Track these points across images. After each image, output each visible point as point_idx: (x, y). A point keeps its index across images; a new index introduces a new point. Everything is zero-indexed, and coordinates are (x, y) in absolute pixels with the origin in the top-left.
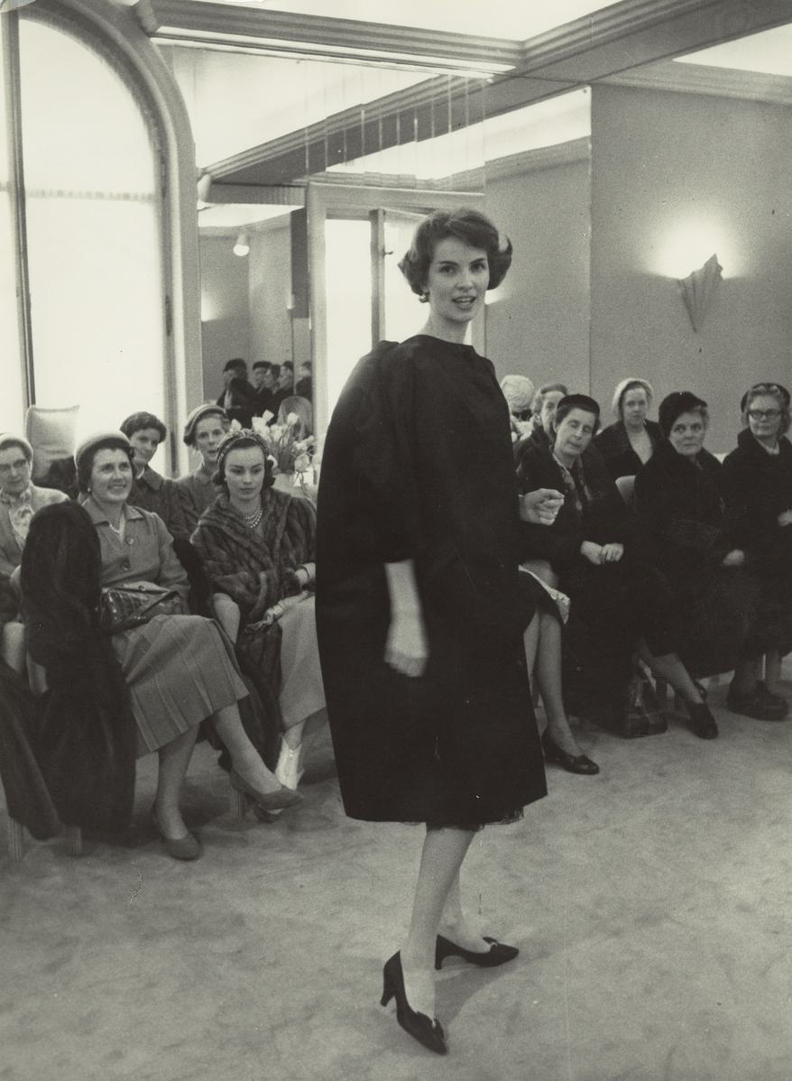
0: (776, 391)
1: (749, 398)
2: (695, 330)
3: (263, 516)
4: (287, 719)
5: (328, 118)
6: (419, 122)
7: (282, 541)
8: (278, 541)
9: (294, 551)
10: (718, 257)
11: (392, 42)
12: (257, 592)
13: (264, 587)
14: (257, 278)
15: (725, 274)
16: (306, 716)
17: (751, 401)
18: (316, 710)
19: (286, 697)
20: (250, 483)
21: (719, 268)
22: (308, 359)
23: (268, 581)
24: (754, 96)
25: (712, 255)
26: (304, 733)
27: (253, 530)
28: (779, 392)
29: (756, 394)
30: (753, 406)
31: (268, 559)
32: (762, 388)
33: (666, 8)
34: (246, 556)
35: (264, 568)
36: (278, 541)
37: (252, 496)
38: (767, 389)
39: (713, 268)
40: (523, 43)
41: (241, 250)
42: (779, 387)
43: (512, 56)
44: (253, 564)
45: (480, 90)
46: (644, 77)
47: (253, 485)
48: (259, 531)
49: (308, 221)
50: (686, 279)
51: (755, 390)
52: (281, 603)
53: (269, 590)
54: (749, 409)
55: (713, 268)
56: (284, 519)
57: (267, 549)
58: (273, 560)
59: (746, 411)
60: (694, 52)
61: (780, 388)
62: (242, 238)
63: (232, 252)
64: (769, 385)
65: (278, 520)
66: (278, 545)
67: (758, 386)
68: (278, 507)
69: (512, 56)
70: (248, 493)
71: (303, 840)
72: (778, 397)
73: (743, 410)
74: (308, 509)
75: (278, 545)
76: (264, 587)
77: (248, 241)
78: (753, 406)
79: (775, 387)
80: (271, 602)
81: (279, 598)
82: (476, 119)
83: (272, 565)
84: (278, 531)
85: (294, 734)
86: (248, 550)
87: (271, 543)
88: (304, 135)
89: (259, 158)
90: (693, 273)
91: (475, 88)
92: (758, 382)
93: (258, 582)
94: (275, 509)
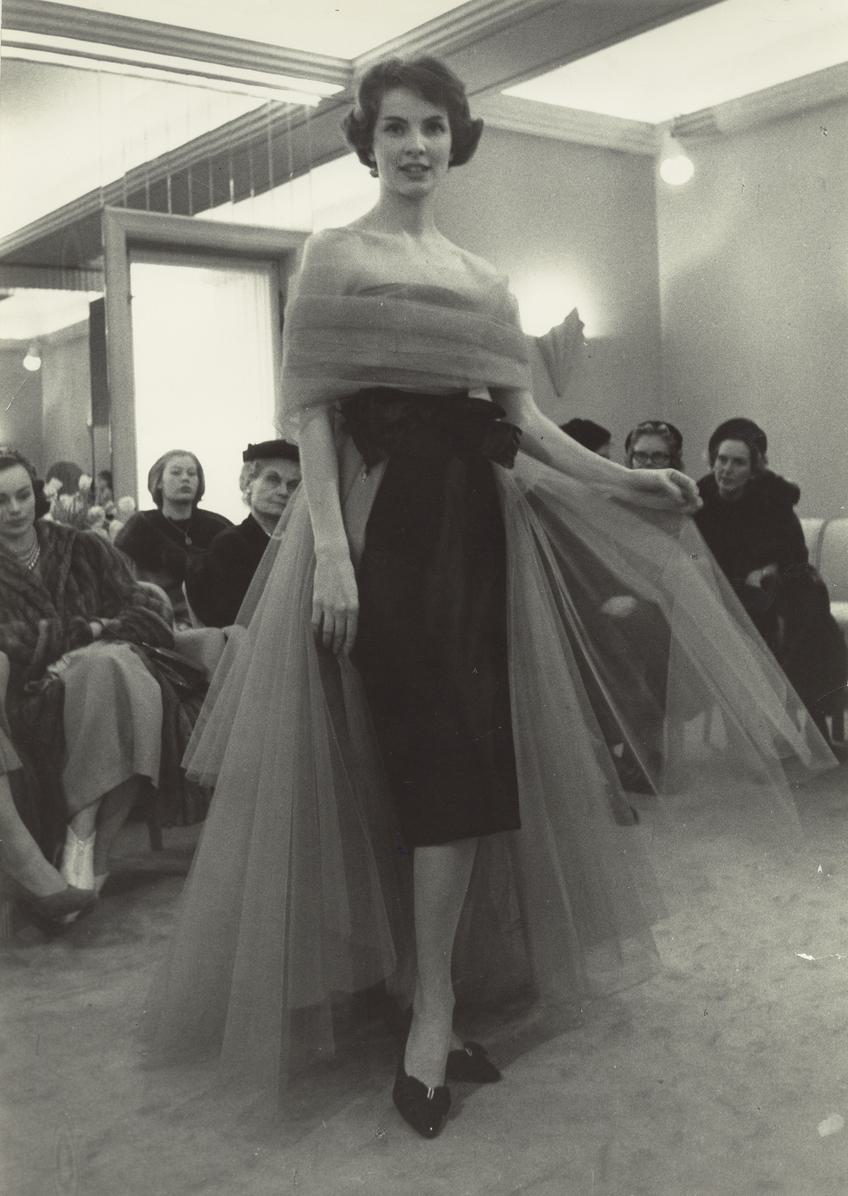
0: (665, 431)
1: (634, 436)
2: (559, 395)
3: (41, 555)
4: (73, 801)
5: (127, 173)
6: (235, 184)
7: (67, 584)
8: (61, 584)
9: (83, 597)
10: (579, 312)
11: (206, 50)
12: (33, 645)
13: (43, 635)
14: (49, 398)
15: (589, 332)
16: (99, 793)
17: (636, 441)
18: (112, 786)
19: (69, 775)
20: (18, 513)
21: (581, 325)
22: (107, 467)
23: (49, 629)
24: (605, 143)
25: (567, 313)
26: (99, 822)
27: (31, 572)
28: (669, 433)
29: (641, 432)
30: (637, 448)
31: (51, 606)
32: (648, 426)
33: (512, 7)
34: (21, 601)
35: (43, 615)
36: (61, 584)
37: (23, 529)
38: (654, 428)
39: (573, 324)
40: (351, 62)
41: (32, 363)
42: (668, 425)
43: (339, 75)
44: (30, 613)
45: (305, 122)
46: (290, 939)
47: (23, 514)
48: (37, 572)
49: (109, 381)
50: (545, 336)
51: (642, 428)
52: (64, 657)
53: (49, 640)
54: (633, 449)
55: (573, 324)
56: (67, 559)
57: (49, 593)
58: (57, 609)
59: (630, 452)
60: (535, 76)
61: (671, 427)
62: (32, 350)
63: (22, 364)
64: (657, 424)
65: (60, 559)
66: (61, 589)
67: (644, 424)
68: (60, 542)
69: (339, 75)
70: (19, 526)
71: (90, 955)
72: (666, 439)
73: (627, 451)
74: (99, 545)
75: (61, 589)
76: (43, 635)
77: (40, 354)
78: (637, 448)
79: (663, 427)
80: (53, 656)
81: (64, 650)
82: (302, 168)
83: (55, 613)
84: (62, 572)
85: (85, 819)
86: (24, 594)
87: (52, 586)
88: (99, 196)
89: (52, 227)
90: (553, 330)
91: (298, 121)
92: (644, 421)
93: (36, 632)
94: (56, 544)
